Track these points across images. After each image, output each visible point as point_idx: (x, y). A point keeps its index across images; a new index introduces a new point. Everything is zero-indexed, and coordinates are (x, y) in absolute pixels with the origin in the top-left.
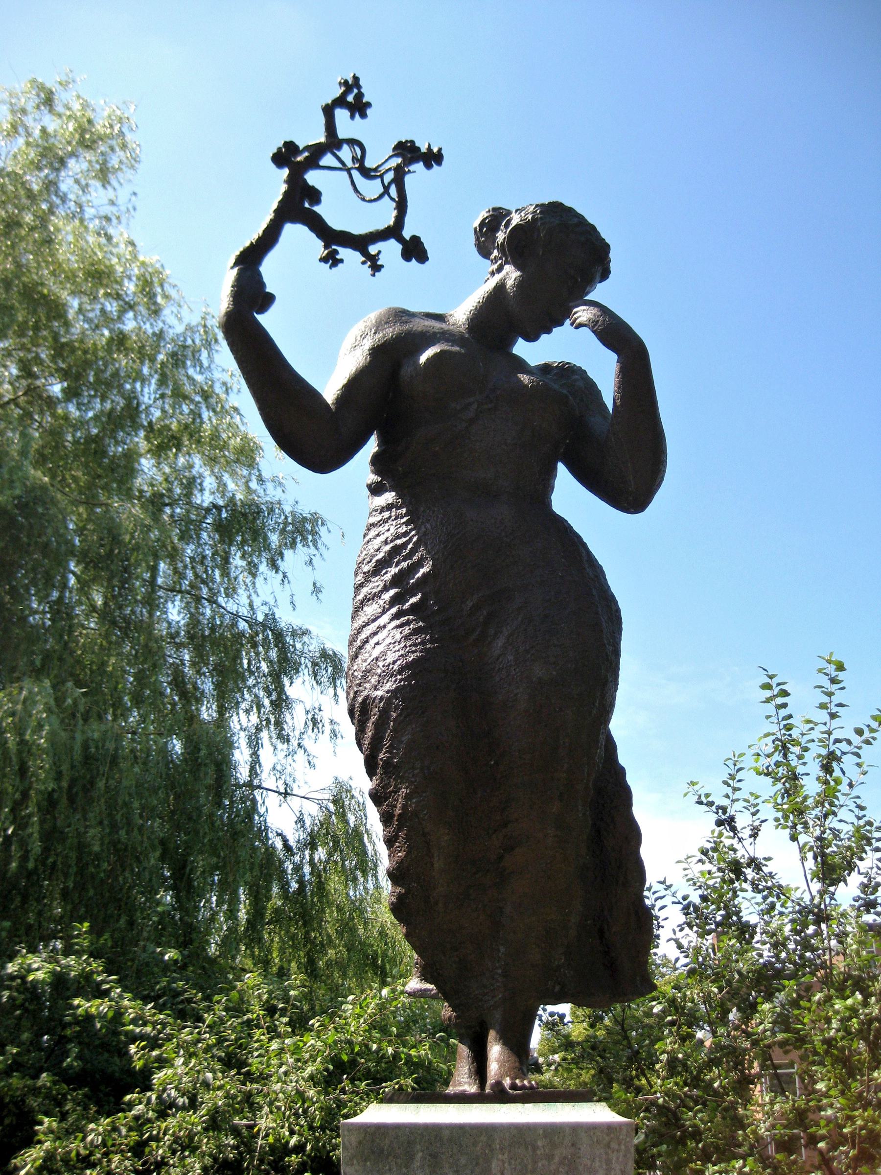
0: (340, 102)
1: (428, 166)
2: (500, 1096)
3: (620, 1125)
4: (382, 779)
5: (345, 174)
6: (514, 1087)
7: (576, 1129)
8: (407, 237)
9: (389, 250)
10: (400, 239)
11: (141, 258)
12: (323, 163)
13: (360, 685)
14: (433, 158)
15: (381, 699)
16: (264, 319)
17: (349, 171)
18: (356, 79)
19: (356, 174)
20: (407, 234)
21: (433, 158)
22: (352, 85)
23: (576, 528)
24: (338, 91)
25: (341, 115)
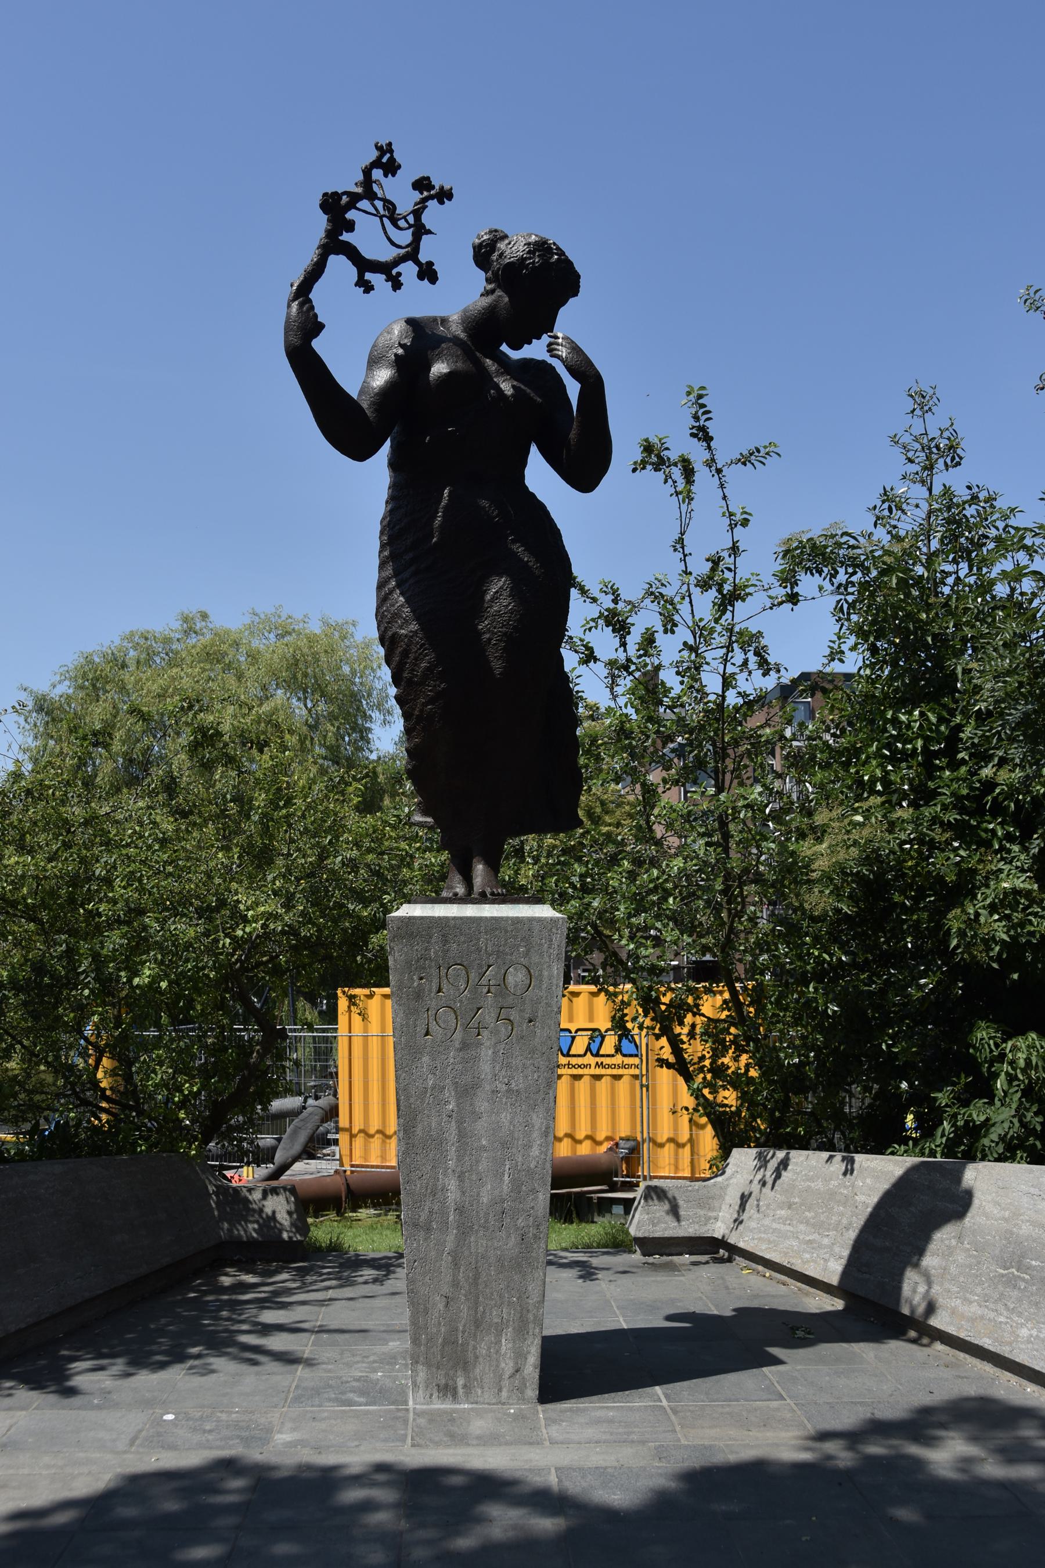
0: (376, 164)
1: (442, 203)
2: (483, 899)
3: (558, 918)
4: (404, 690)
5: (378, 219)
6: (492, 894)
7: (531, 920)
8: (424, 261)
9: (408, 271)
10: (417, 262)
11: (925, 488)
12: (359, 205)
13: (388, 623)
14: (444, 195)
15: (406, 636)
16: (316, 344)
17: (381, 217)
18: (390, 144)
19: (386, 221)
20: (423, 258)
21: (444, 195)
22: (384, 150)
23: (553, 515)
24: (374, 154)
25: (377, 174)
